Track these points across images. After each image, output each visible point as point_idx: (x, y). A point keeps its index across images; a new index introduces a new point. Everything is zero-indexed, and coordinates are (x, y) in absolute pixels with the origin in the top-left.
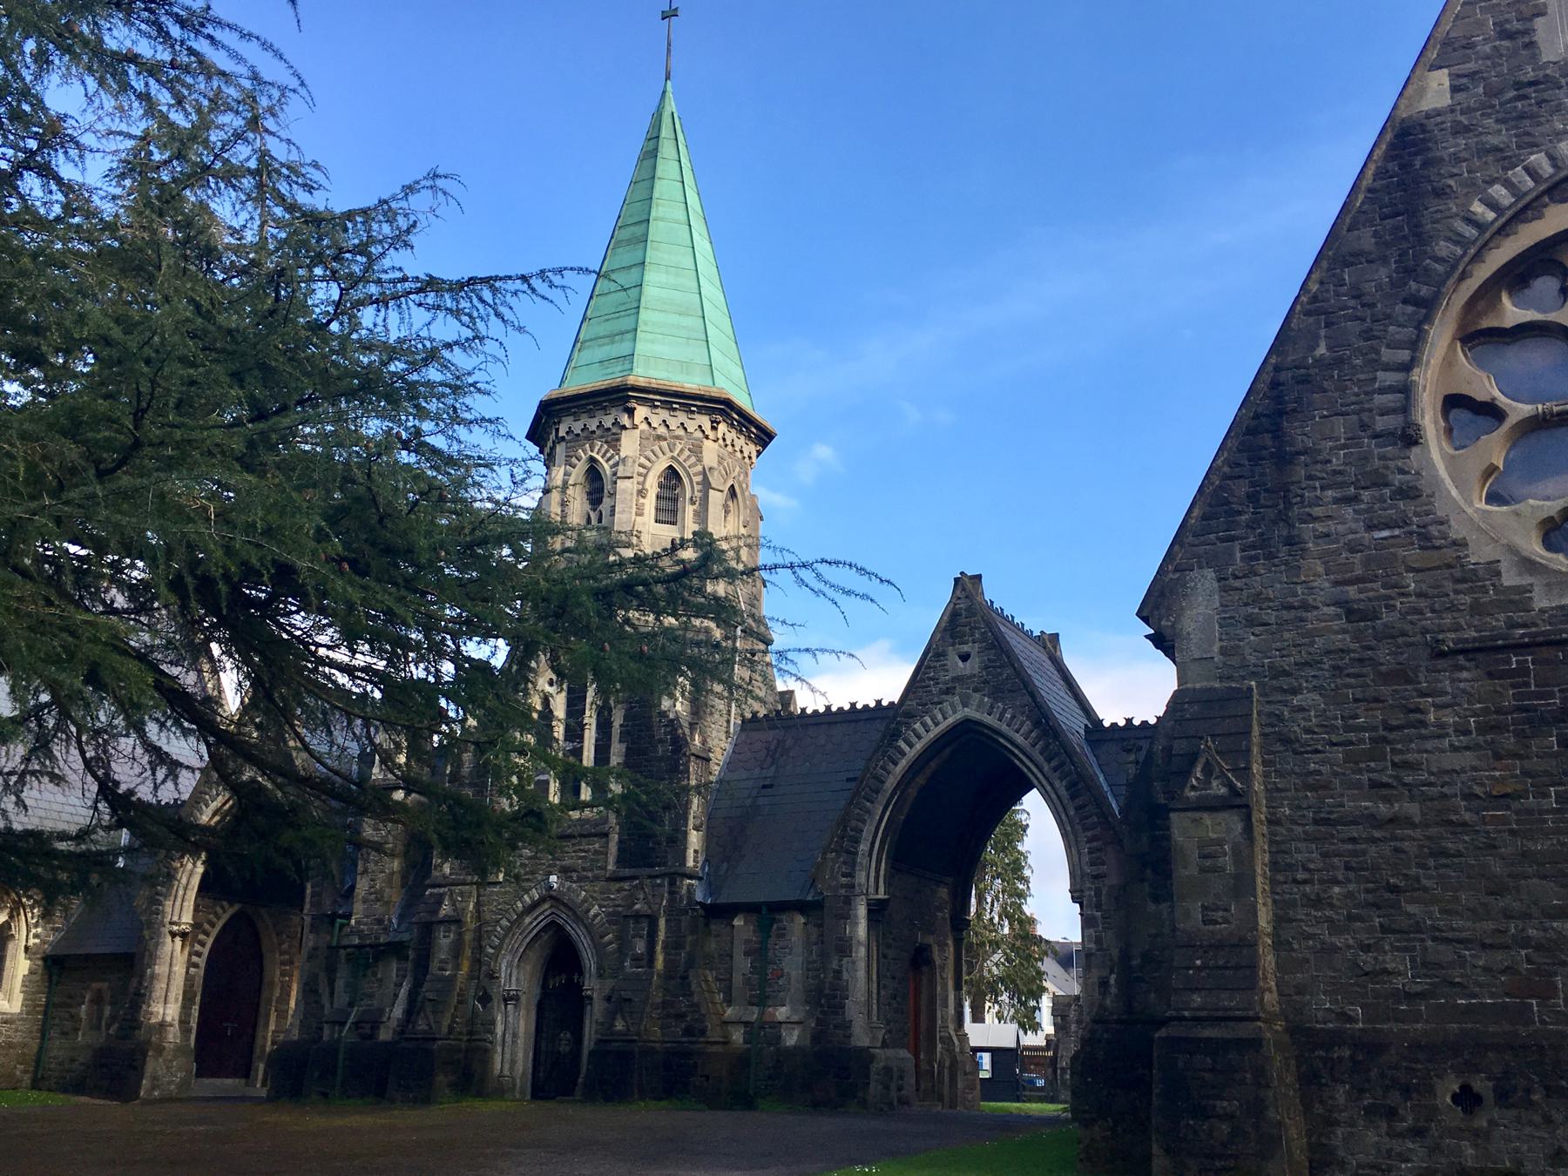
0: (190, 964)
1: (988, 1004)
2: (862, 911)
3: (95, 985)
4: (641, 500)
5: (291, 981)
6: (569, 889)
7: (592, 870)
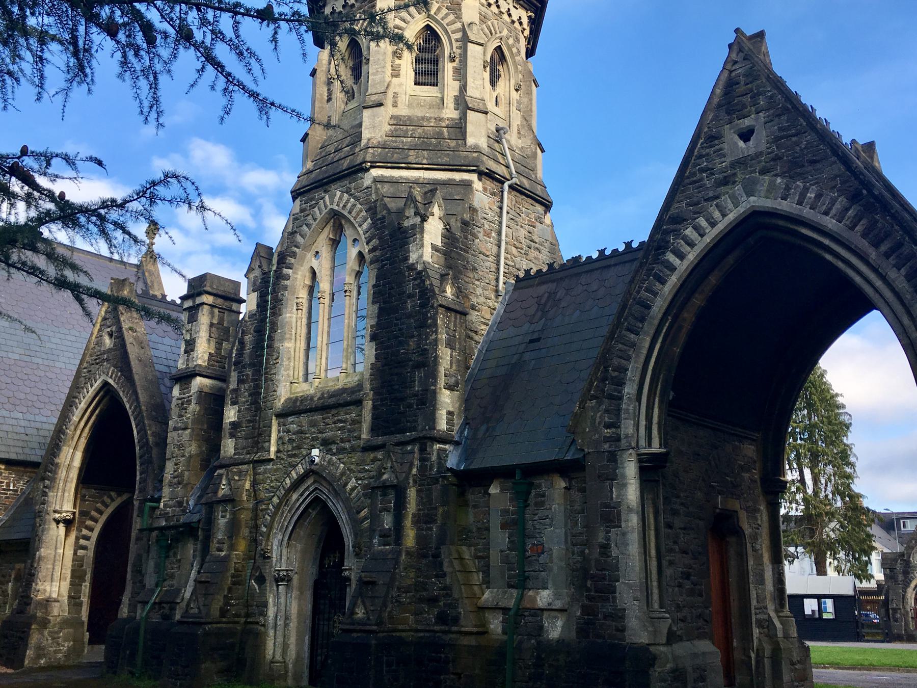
0: (78, 547)
1: (828, 561)
2: (630, 469)
3: (17, 566)
4: (397, 61)
6: (329, 462)
7: (349, 441)
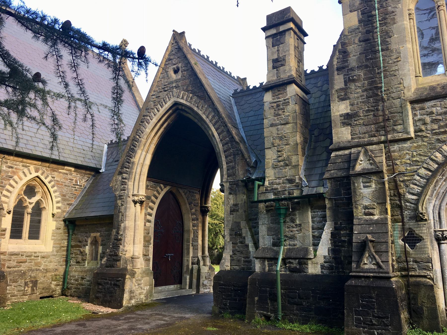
3: (92, 235)
5: (197, 230)
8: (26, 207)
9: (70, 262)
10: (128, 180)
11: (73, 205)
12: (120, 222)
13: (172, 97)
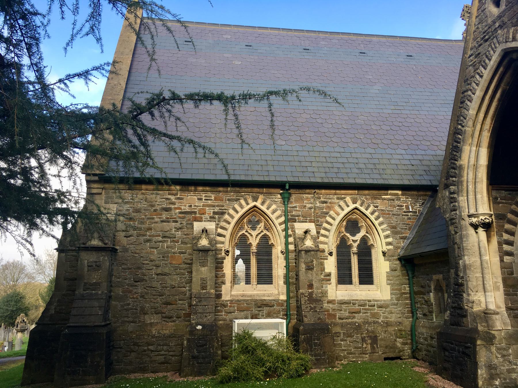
3: (435, 277)
8: (350, 246)
9: (417, 314)
10: (458, 195)
11: (409, 239)
12: (458, 259)
13: (497, 45)
